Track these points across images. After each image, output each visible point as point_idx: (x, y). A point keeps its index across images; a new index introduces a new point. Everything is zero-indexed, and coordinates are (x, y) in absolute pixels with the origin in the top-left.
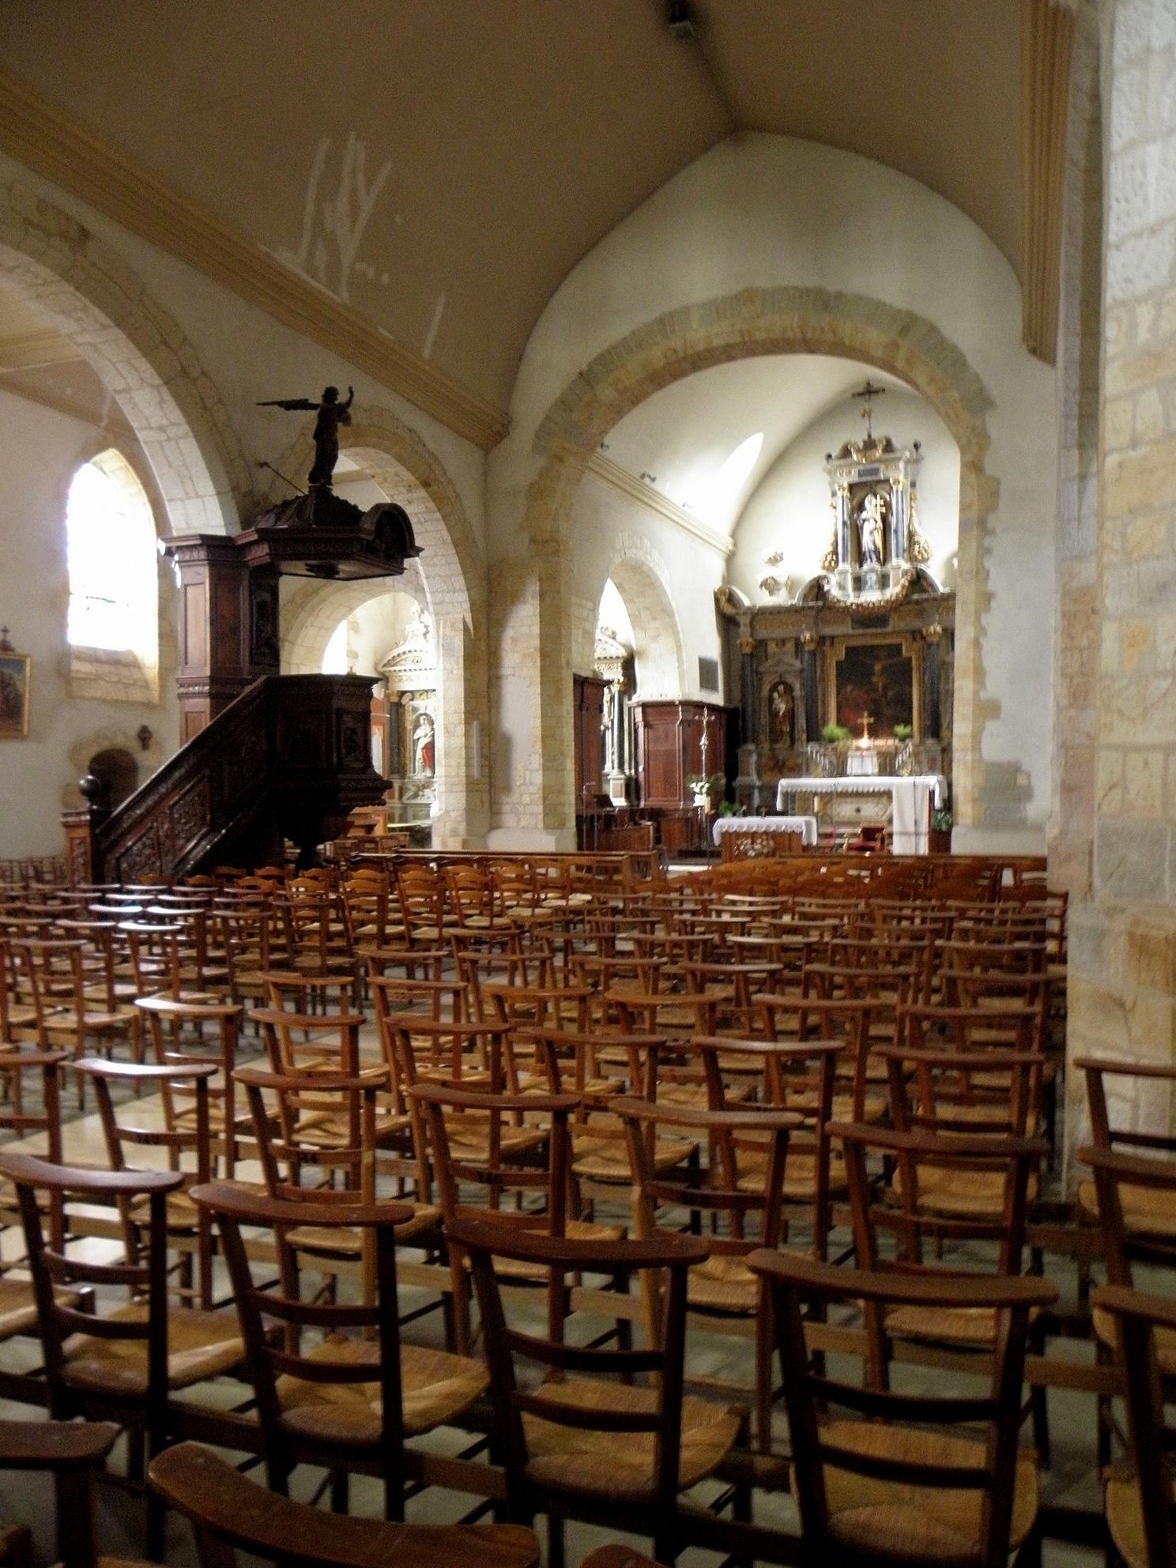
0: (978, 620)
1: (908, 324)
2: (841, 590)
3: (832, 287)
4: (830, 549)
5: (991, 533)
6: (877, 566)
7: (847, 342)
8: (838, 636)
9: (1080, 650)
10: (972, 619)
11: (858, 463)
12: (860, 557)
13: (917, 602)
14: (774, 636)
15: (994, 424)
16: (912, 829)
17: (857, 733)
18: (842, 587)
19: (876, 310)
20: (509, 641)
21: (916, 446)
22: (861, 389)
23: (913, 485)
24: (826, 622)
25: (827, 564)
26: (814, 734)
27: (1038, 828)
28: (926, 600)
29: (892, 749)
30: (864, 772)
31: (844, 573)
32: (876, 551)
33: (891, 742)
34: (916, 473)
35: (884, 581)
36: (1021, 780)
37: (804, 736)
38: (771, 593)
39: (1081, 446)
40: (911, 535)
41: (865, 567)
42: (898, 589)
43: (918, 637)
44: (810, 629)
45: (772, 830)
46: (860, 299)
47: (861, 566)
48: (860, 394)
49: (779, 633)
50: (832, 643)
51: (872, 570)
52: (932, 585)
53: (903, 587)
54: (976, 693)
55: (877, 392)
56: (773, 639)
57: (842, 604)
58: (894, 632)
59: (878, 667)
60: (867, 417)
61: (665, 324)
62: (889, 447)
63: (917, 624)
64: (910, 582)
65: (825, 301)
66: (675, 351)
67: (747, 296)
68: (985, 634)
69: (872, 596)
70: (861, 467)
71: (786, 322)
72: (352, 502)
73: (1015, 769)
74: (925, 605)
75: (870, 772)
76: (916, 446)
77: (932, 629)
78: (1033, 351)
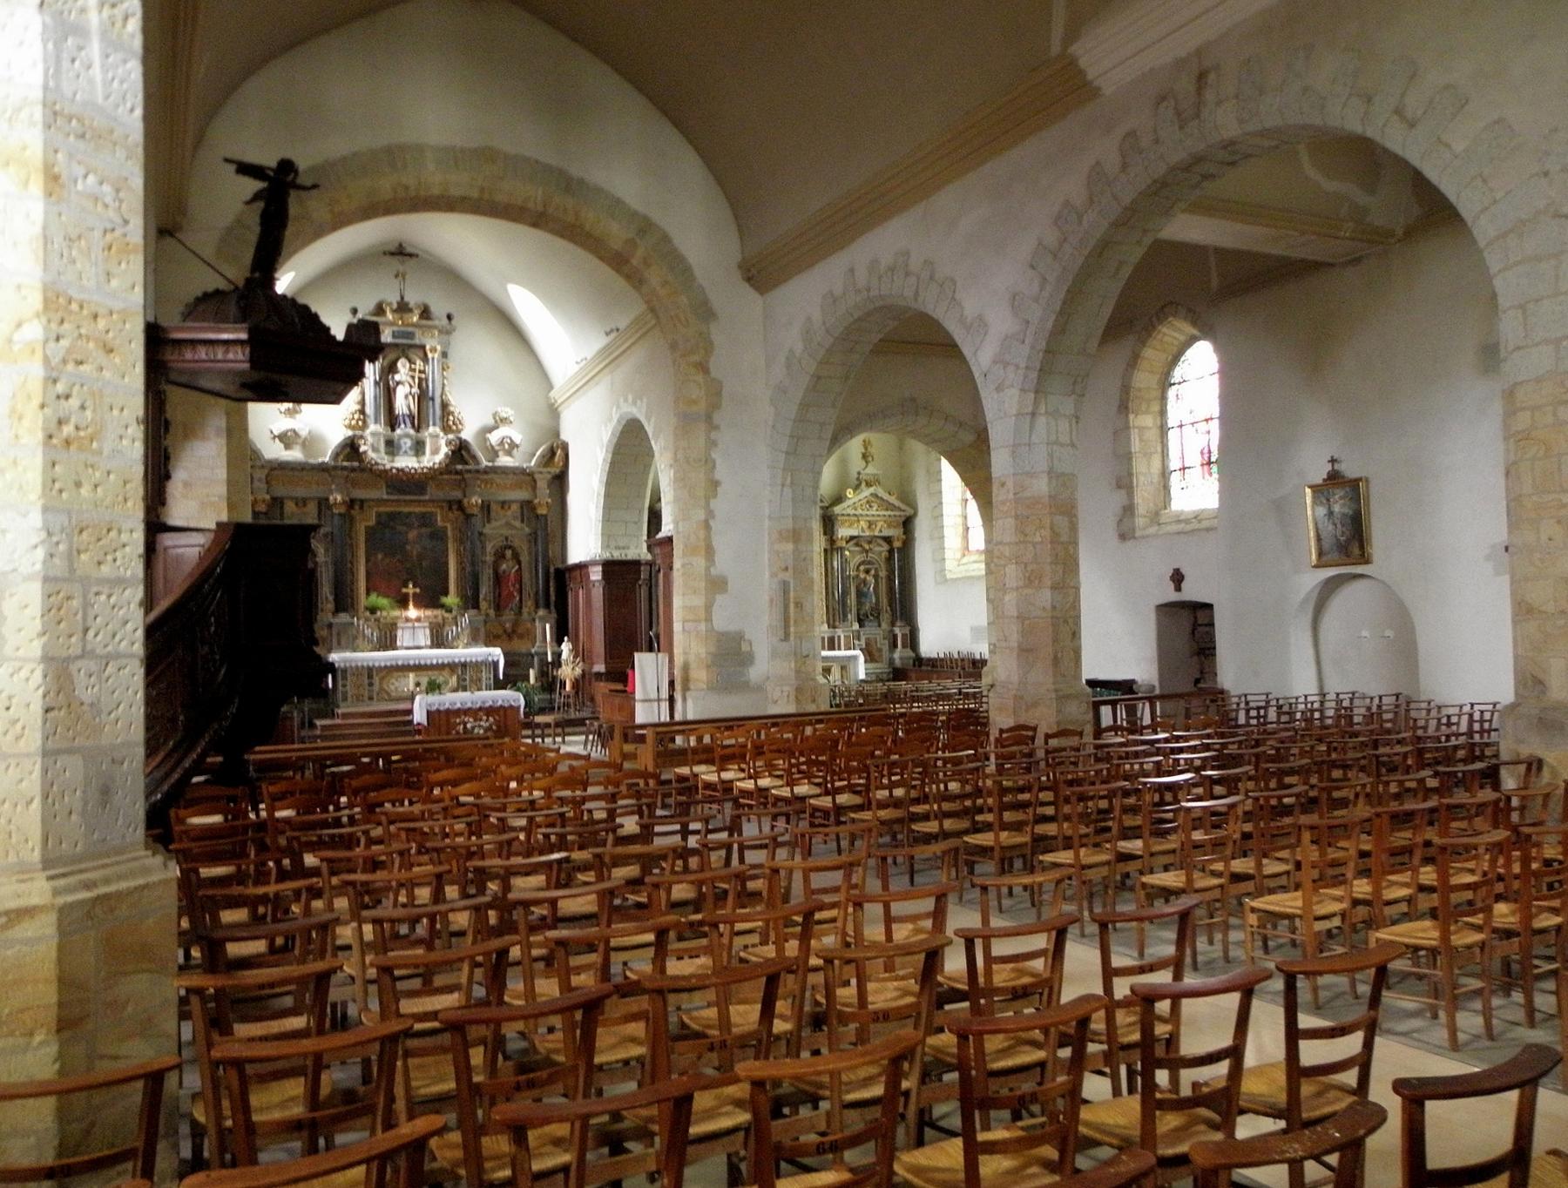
0: (708, 504)
1: (645, 226)
2: (372, 450)
3: (575, 171)
4: (358, 407)
5: (717, 428)
6: (412, 432)
7: (587, 227)
8: (366, 500)
9: (1034, 545)
10: (702, 503)
11: (392, 324)
12: (392, 421)
13: (457, 473)
14: (294, 494)
15: (718, 335)
16: (654, 695)
17: (403, 602)
18: (375, 449)
19: (616, 205)
20: (180, 485)
21: (449, 317)
22: (392, 248)
23: (444, 355)
24: (355, 484)
25: (353, 422)
26: (344, 602)
27: (759, 689)
28: (469, 471)
29: (440, 619)
30: (416, 644)
31: (373, 434)
32: (411, 416)
33: (438, 612)
34: (446, 345)
35: (419, 447)
36: (745, 647)
37: (331, 606)
38: (288, 447)
39: (1036, 392)
40: (445, 406)
41: (398, 431)
42: (439, 457)
43: (455, 507)
44: (342, 493)
45: (487, 705)
46: (599, 190)
47: (393, 430)
48: (392, 254)
49: (300, 492)
50: (361, 507)
51: (407, 436)
52: (474, 457)
53: (447, 455)
54: (708, 569)
55: (411, 255)
56: (291, 498)
57: (381, 467)
58: (430, 501)
59: (412, 535)
60: (400, 278)
61: (394, 155)
62: (426, 313)
63: (457, 494)
64: (453, 452)
65: (570, 185)
66: (407, 188)
67: (487, 155)
68: (713, 517)
69: (406, 462)
70: (395, 328)
71: (530, 193)
72: (313, 309)
73: (739, 637)
74: (467, 476)
75: (423, 644)
76: (449, 317)
77: (473, 501)
78: (749, 280)
